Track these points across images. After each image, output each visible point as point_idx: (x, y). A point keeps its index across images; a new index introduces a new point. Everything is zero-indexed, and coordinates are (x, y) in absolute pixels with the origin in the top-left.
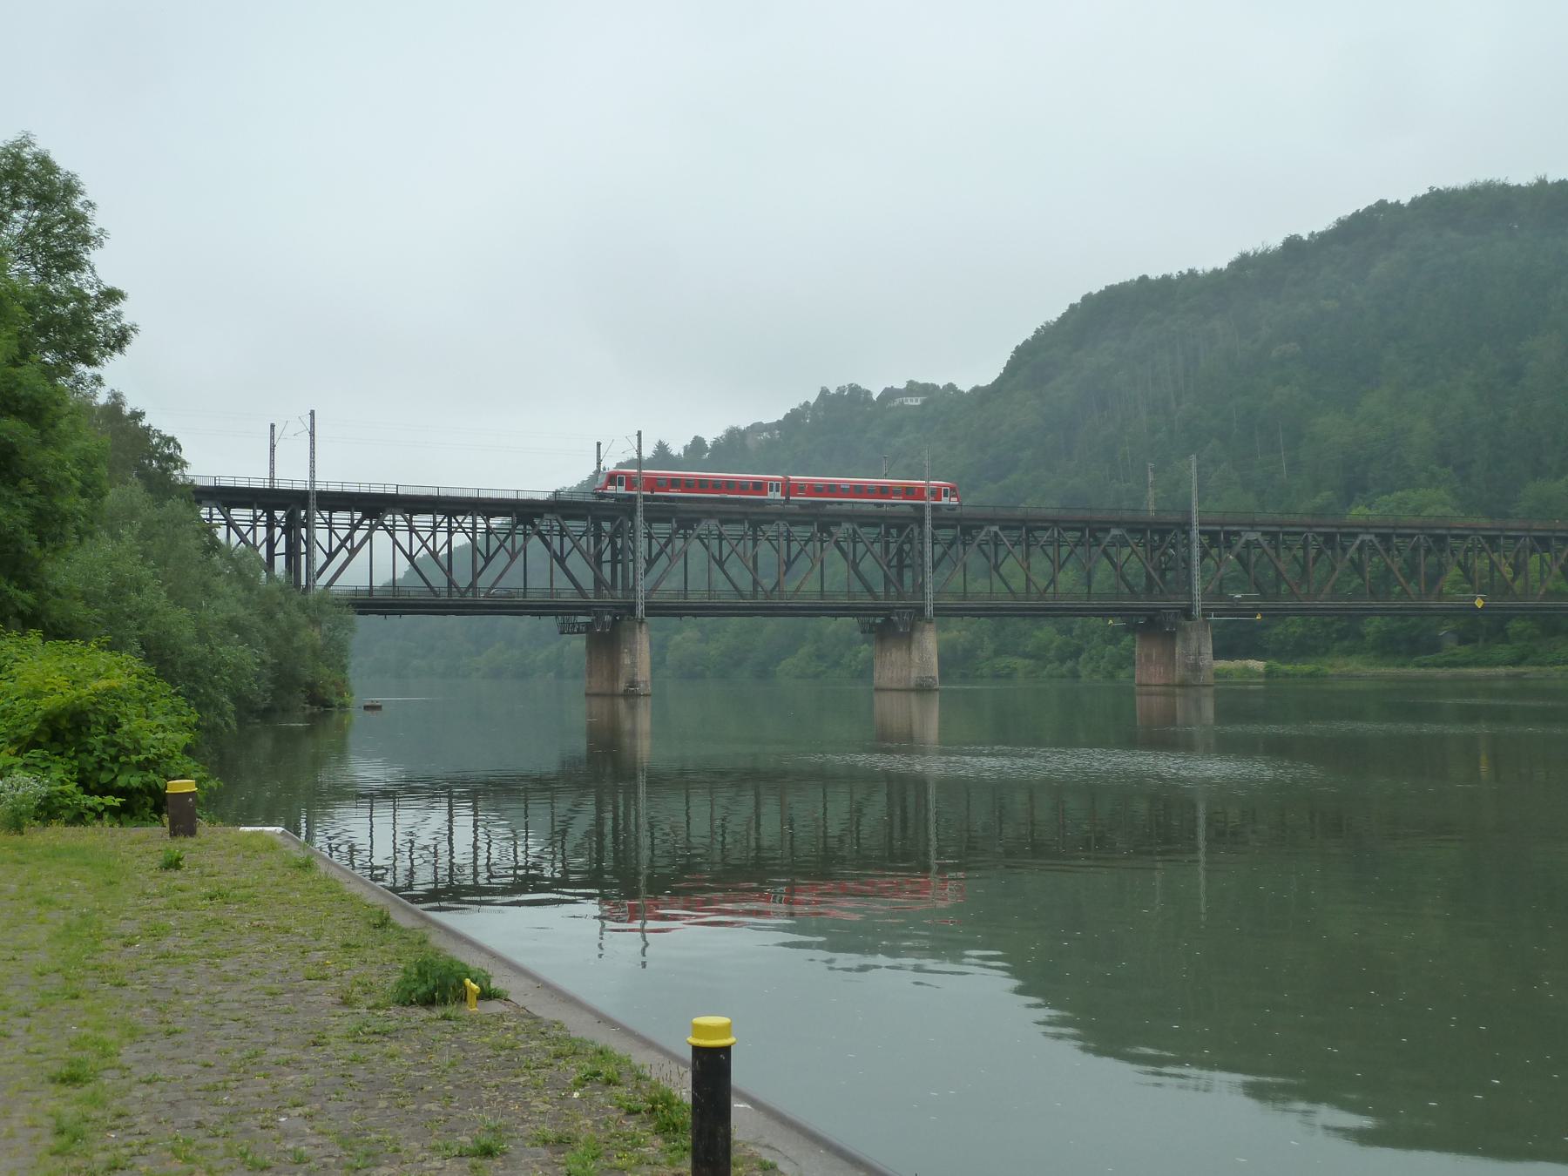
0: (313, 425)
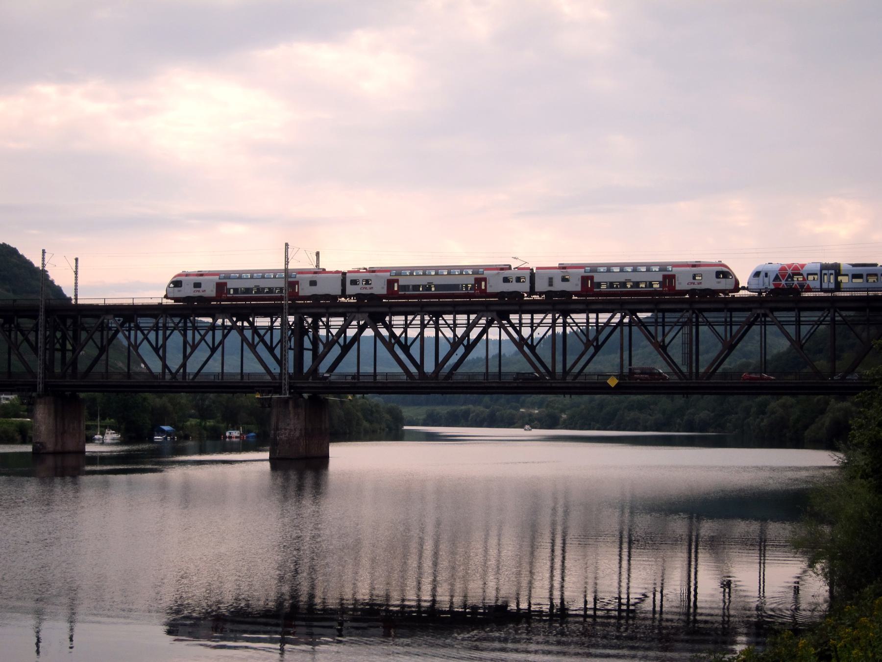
0: (77, 267)
